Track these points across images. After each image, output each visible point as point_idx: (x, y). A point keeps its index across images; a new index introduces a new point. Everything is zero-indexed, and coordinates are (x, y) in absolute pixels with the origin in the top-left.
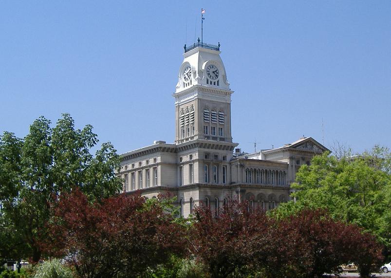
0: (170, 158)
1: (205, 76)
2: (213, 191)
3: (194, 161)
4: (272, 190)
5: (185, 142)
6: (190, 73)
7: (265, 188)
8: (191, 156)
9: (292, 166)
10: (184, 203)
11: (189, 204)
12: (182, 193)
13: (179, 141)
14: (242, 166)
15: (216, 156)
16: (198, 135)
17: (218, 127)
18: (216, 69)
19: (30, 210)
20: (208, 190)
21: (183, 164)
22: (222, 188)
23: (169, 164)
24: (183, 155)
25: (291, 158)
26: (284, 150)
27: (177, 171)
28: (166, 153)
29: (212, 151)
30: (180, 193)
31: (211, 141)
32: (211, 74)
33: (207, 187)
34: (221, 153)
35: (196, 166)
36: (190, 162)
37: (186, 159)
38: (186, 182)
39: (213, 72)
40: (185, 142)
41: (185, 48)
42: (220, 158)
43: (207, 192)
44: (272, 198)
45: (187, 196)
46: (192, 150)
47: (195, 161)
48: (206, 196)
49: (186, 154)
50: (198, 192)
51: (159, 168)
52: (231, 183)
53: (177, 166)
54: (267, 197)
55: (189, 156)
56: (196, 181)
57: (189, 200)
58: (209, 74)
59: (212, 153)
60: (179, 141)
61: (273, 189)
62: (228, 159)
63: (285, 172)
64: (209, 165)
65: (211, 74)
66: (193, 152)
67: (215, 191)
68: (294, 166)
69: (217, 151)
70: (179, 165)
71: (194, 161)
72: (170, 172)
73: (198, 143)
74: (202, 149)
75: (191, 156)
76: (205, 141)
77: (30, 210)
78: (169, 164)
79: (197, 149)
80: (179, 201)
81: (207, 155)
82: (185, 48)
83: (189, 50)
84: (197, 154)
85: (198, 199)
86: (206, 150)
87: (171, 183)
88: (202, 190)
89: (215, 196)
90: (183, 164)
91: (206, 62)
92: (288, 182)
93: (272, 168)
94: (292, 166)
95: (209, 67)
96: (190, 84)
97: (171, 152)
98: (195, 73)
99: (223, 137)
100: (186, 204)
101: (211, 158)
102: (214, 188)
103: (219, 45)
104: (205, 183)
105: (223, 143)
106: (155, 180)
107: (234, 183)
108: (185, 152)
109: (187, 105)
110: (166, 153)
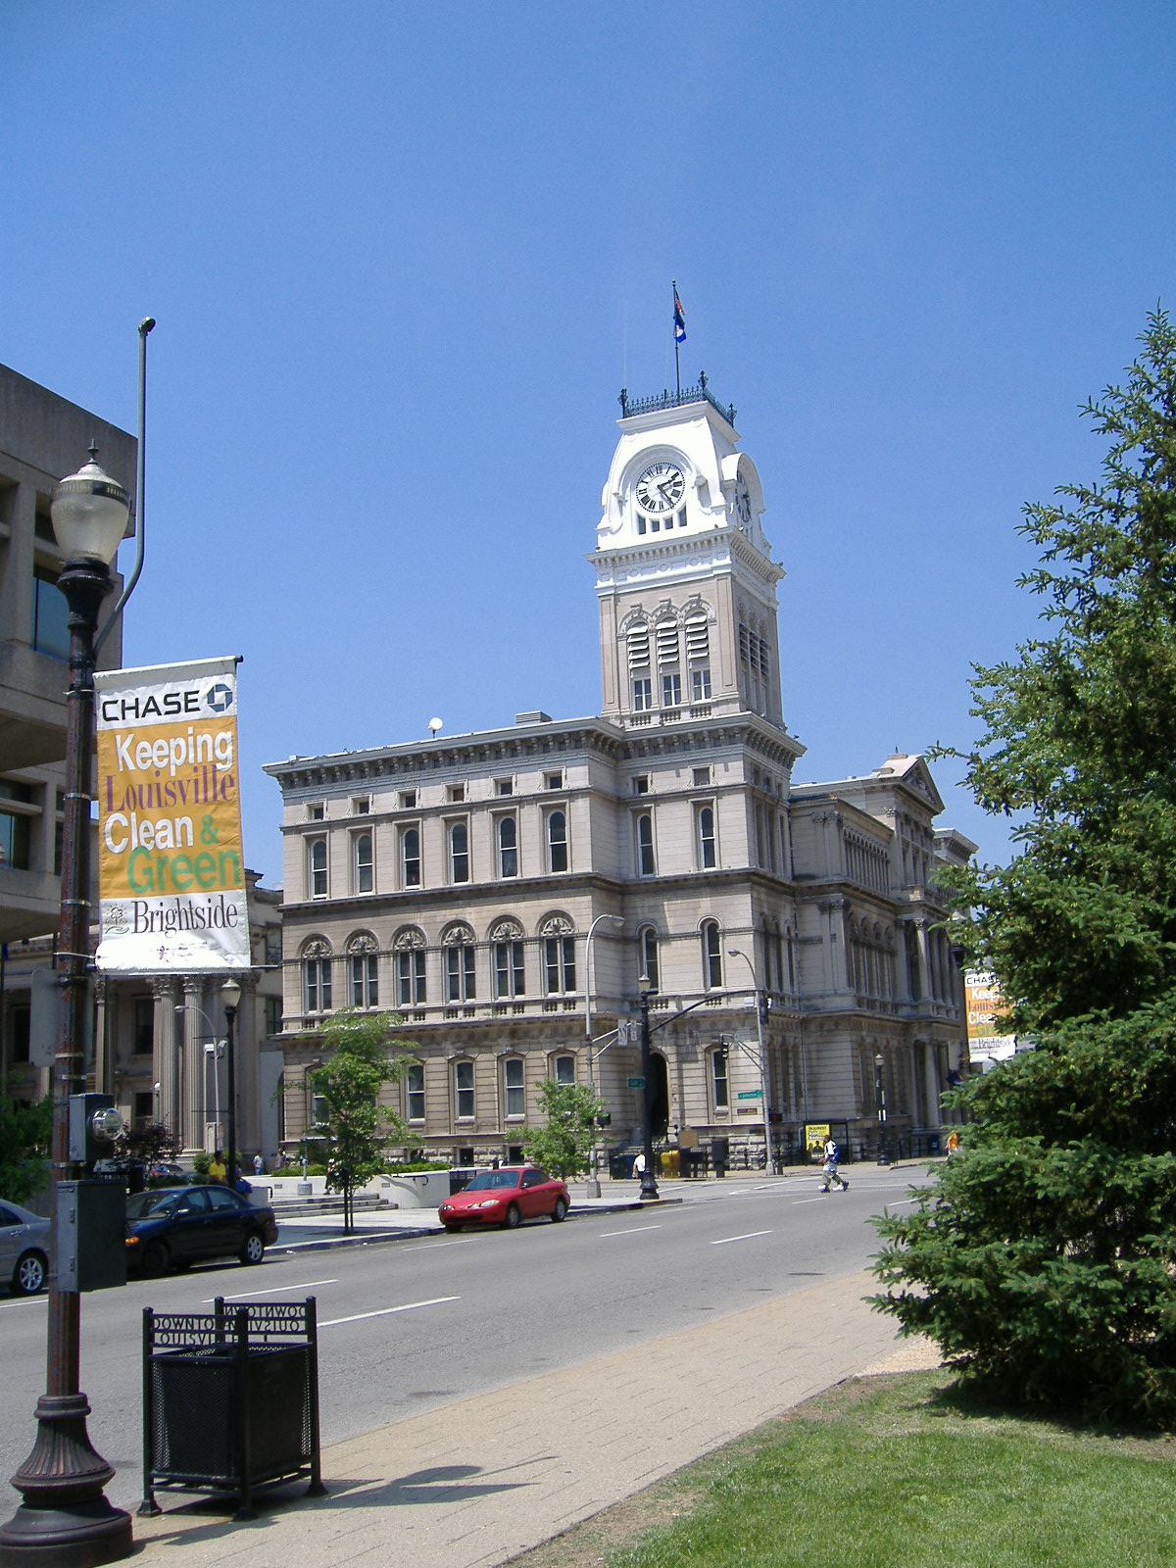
5: (655, 721)
8: (701, 775)
10: (667, 938)
11: (698, 943)
12: (650, 902)
41: (623, 399)
45: (679, 915)
46: (323, 788)
47: (731, 789)
49: (677, 767)
55: (688, 774)
57: (695, 928)
66: (713, 759)
75: (701, 775)
82: (623, 399)
109: (664, 595)
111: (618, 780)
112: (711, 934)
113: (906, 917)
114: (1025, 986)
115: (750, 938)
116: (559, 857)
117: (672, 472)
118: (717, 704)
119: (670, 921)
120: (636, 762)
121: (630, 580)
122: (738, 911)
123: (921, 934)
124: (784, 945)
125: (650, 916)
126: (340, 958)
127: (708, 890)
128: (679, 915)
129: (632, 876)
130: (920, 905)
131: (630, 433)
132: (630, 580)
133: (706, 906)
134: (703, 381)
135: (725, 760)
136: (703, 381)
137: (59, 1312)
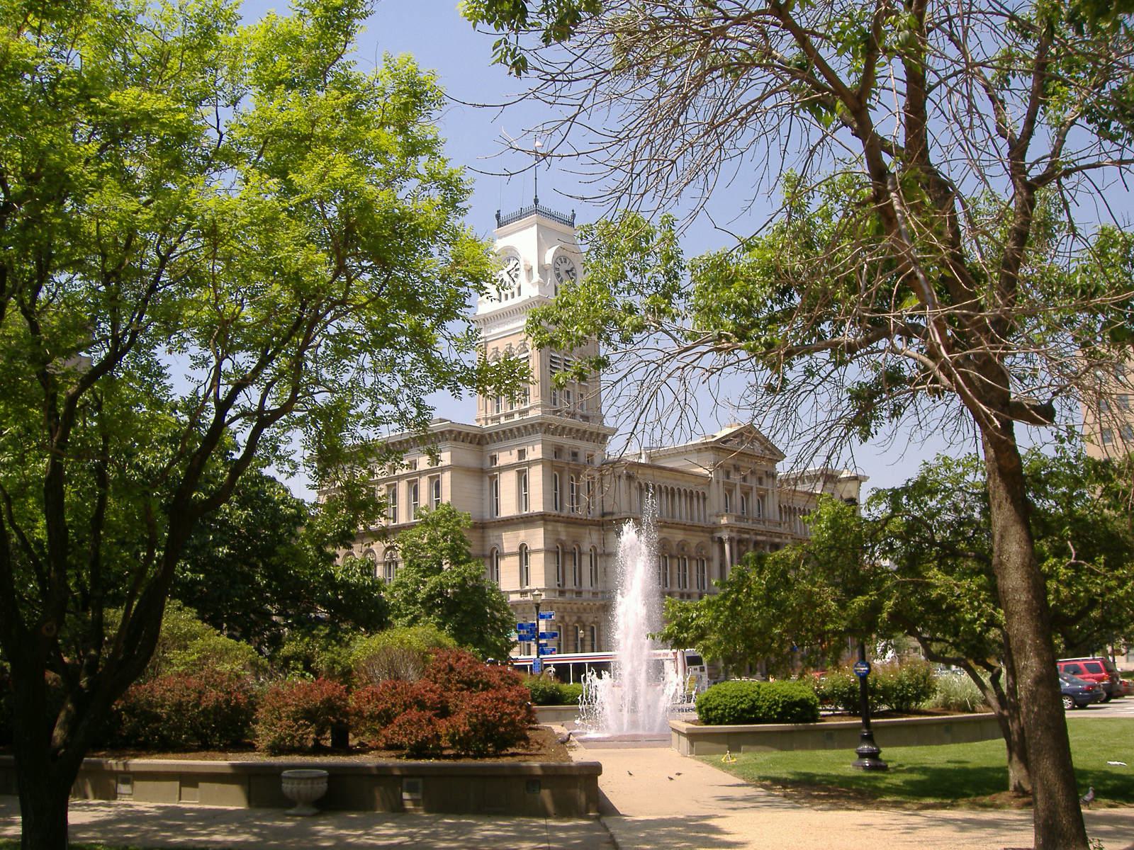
0: (469, 457)
1: (551, 279)
2: (571, 530)
3: (530, 464)
4: (682, 532)
5: (517, 418)
6: (517, 270)
7: (671, 528)
8: (522, 453)
9: (718, 482)
10: (503, 556)
11: (517, 558)
12: (496, 533)
13: (486, 419)
14: (630, 477)
15: (575, 455)
16: (542, 406)
17: (577, 391)
18: (571, 266)
19: (59, 221)
20: (561, 527)
21: (501, 469)
22: (587, 525)
23: (468, 470)
24: (500, 450)
25: (716, 467)
26: (701, 449)
27: (482, 485)
28: (460, 444)
29: (565, 441)
30: (492, 534)
31: (568, 421)
32: (563, 275)
33: (558, 521)
34: (584, 447)
35: (536, 477)
36: (519, 465)
37: (506, 458)
38: (508, 507)
39: (567, 272)
40: (517, 418)
41: (498, 217)
42: (582, 459)
43: (558, 533)
44: (683, 549)
45: (510, 541)
46: (525, 439)
47: (535, 462)
48: (557, 540)
49: (510, 449)
50: (542, 530)
51: (446, 478)
52: (604, 515)
53: (486, 475)
54: (675, 547)
55: (515, 452)
56: (537, 505)
57: (516, 549)
58: (558, 275)
59: (566, 446)
60: (486, 419)
61: (684, 529)
62: (597, 462)
63: (704, 493)
64: (561, 473)
65: (563, 275)
66: (527, 444)
67: (572, 530)
68: (721, 483)
69: (578, 443)
70: (487, 472)
71: (530, 464)
72: (470, 485)
73: (541, 424)
74: (549, 437)
75: (522, 453)
76: (556, 420)
77: (59, 221)
78: (468, 470)
79: (539, 436)
80: (488, 553)
81: (558, 451)
82: (498, 217)
83: (507, 223)
84: (539, 447)
85: (541, 545)
86: (557, 439)
87: (468, 511)
88: (550, 528)
89: (574, 541)
90: (501, 469)
91: (555, 248)
92: (710, 516)
93: (684, 485)
94: (718, 482)
95: (560, 259)
96: (516, 294)
97: (470, 442)
98: (530, 271)
99: (585, 412)
100: (508, 559)
101: (567, 457)
102: (575, 523)
103: (574, 216)
104: (555, 512)
105: (585, 426)
106: (523, 498)
107: (612, 514)
108: (505, 444)
109: (508, 341)
110: (468, 445)
111: (482, 458)
112: (523, 553)
113: (718, 535)
114: (844, 583)
115: (542, 555)
116: (523, 498)
117: (516, 262)
118: (531, 408)
119: (505, 545)
120: (492, 446)
121: (493, 332)
122: (536, 538)
123: (727, 547)
124: (586, 560)
125: (497, 542)
126: (380, 563)
127: (523, 526)
128: (510, 541)
129: (488, 517)
130: (726, 526)
131: (500, 238)
132: (493, 332)
133: (522, 535)
134: (536, 201)
135: (533, 443)
136: (536, 201)
137: (895, 802)
